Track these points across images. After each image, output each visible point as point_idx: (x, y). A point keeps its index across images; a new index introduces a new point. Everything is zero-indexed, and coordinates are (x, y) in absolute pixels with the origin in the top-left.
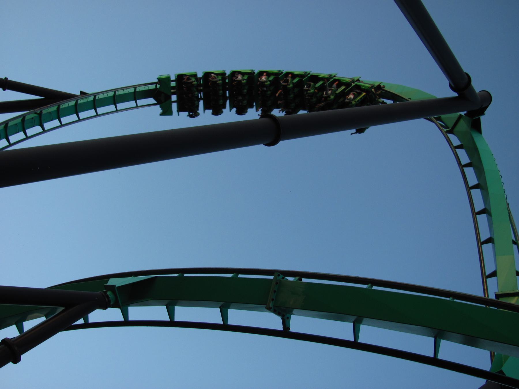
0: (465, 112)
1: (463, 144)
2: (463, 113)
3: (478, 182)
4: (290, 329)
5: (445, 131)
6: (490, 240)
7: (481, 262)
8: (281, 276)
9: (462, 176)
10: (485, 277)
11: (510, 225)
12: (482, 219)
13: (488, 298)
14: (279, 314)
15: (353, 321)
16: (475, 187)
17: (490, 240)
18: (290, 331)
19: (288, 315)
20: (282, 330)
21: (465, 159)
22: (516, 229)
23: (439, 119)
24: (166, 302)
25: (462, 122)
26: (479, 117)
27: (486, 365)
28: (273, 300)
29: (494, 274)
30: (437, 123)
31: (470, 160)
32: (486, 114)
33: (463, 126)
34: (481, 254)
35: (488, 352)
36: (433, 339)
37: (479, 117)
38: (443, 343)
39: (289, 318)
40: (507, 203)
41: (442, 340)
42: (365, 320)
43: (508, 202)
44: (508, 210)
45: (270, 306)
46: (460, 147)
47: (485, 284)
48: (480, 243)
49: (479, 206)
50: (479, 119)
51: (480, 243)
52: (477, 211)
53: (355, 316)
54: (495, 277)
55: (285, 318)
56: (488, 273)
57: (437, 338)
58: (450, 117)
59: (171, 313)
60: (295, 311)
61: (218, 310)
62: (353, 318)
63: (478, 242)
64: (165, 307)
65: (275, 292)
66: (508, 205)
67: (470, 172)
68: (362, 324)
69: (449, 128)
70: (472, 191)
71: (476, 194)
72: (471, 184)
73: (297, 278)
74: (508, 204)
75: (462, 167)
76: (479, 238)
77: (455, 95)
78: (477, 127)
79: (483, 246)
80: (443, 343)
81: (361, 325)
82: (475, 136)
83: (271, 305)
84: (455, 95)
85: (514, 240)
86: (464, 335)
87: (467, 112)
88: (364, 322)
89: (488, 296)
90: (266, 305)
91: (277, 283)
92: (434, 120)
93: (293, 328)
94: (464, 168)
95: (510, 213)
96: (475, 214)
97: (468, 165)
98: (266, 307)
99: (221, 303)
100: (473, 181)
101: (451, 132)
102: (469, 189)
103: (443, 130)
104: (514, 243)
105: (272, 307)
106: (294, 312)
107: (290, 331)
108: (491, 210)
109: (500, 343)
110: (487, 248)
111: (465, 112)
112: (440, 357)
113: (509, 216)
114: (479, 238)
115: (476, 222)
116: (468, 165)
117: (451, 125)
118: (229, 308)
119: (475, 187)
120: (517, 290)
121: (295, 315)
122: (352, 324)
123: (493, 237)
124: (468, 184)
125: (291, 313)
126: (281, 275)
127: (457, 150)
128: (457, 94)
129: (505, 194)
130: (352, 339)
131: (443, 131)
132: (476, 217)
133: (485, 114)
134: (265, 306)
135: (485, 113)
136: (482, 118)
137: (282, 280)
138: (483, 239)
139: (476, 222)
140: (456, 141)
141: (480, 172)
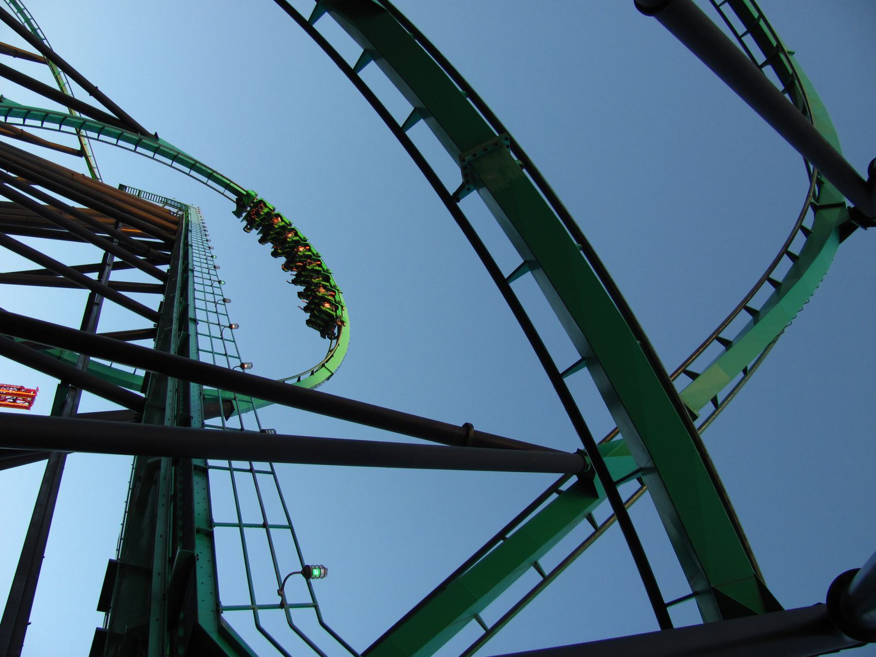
0: (852, 206)
1: (811, 232)
2: (849, 204)
3: (782, 282)
4: (459, 201)
5: (812, 201)
6: (727, 344)
7: (703, 347)
8: (508, 143)
9: (776, 259)
10: (683, 370)
11: (761, 353)
12: (744, 318)
13: (671, 381)
14: (465, 175)
15: (527, 259)
16: (774, 283)
17: (727, 344)
18: (457, 203)
19: (471, 187)
20: (451, 194)
21: (796, 248)
22: (761, 361)
23: (820, 184)
24: (370, 46)
25: (837, 211)
26: (858, 225)
27: (597, 437)
28: (475, 155)
29: (693, 376)
30: (813, 185)
31: (800, 254)
32: (867, 231)
33: (834, 216)
34: (705, 346)
35: (615, 426)
36: (579, 358)
37: (858, 225)
38: (584, 372)
39: (469, 191)
40: (783, 330)
41: (586, 367)
42: (540, 272)
43: (785, 330)
44: (776, 337)
45: (466, 158)
46: (806, 232)
47: (676, 375)
48: (715, 336)
49: (756, 303)
50: (856, 228)
51: (716, 336)
52: (748, 305)
53: (534, 255)
54: (692, 380)
55: (467, 186)
56: (690, 368)
57: (584, 361)
58: (833, 193)
59: (362, 63)
60: (484, 190)
61: (411, 109)
62: (531, 257)
63: (683, 366)
64: (362, 50)
65: (485, 150)
66: (782, 333)
67: (786, 264)
68: (532, 272)
69: (818, 203)
70: (767, 283)
71: (768, 290)
72: (772, 276)
73: (520, 162)
74: (783, 332)
75: (785, 251)
76: (720, 330)
77: (865, 177)
78: (844, 231)
79: (683, 375)
80: (584, 372)
81: (529, 273)
82: (833, 238)
83: (467, 158)
84: (865, 177)
85: (748, 369)
86: (611, 383)
87: (854, 207)
88: (535, 272)
89: (673, 380)
90: (463, 153)
91: (496, 144)
92: (815, 179)
93: (463, 205)
94: (785, 256)
95: (774, 341)
96: (744, 306)
97: (792, 256)
98: (460, 155)
99: (423, 106)
100: (779, 275)
101: (815, 209)
102: (767, 277)
103: (810, 198)
104: (745, 371)
105: (467, 161)
106: (481, 190)
107: (457, 203)
108: (762, 318)
109: (635, 430)
110: (716, 347)
111: (852, 206)
112: (567, 380)
113: (770, 344)
114: (720, 330)
115: (735, 314)
116: (792, 256)
117: (823, 202)
118: (423, 119)
119: (774, 283)
120: (697, 411)
121: (479, 193)
122: (523, 261)
123: (733, 344)
124: (771, 273)
125: (477, 187)
126: (509, 141)
127: (800, 232)
128: (868, 179)
129: (792, 321)
130: (506, 275)
131: (809, 200)
132: (741, 309)
133: (866, 229)
134: (461, 153)
135: (868, 228)
136: (860, 230)
137: (505, 147)
138: (722, 335)
139: (735, 314)
140: (809, 222)
141: (795, 275)
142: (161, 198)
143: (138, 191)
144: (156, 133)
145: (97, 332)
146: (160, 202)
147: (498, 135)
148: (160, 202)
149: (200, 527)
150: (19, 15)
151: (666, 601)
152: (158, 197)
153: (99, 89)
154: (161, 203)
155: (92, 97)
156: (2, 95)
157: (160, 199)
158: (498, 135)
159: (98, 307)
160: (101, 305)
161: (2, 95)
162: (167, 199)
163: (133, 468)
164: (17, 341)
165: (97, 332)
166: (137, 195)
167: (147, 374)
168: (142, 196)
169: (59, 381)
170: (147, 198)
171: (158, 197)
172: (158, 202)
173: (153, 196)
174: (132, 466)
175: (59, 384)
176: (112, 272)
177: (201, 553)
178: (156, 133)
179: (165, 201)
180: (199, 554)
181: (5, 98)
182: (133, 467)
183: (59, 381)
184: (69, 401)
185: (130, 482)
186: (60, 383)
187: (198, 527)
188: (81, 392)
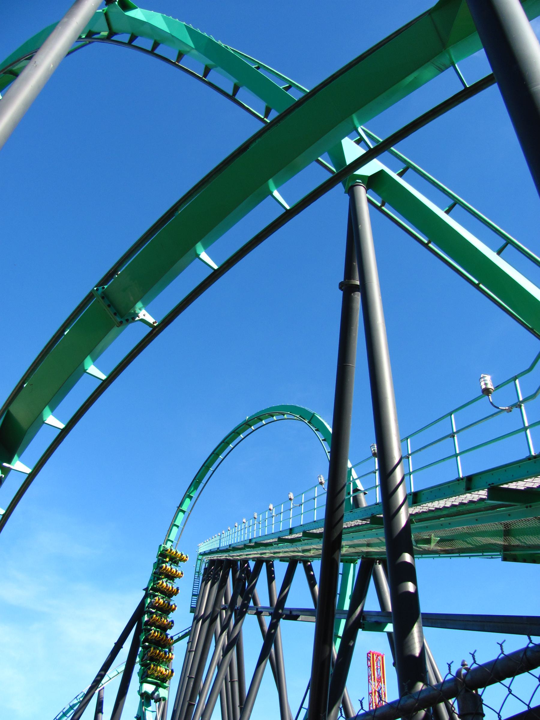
94: (156, 52)
98: (117, 326)
127: (133, 44)
137: (104, 290)
138: (230, 93)
142: (196, 578)
143: (193, 597)
144: (144, 590)
145: (313, 607)
146: (199, 578)
147: (96, 298)
148: (199, 578)
149: (465, 488)
150: (68, 715)
151: (463, 88)
152: (195, 580)
153: (121, 649)
154: (200, 577)
155: (123, 646)
156: (135, 717)
157: (197, 578)
158: (96, 298)
159: (294, 611)
160: (290, 609)
161: (135, 717)
162: (195, 573)
163: (422, 557)
164: (332, 672)
165: (313, 607)
166: (196, 597)
167: (341, 562)
168: (197, 593)
169: (360, 630)
170: (197, 589)
171: (195, 580)
172: (199, 579)
173: (195, 584)
174: (420, 559)
175: (362, 630)
176: (235, 97)
177: (486, 483)
178: (144, 590)
179: (198, 574)
180: (488, 484)
181: (137, 715)
182: (420, 557)
183: (360, 630)
184: (374, 619)
185: (433, 557)
186: (361, 629)
187: (465, 489)
188: (365, 611)
